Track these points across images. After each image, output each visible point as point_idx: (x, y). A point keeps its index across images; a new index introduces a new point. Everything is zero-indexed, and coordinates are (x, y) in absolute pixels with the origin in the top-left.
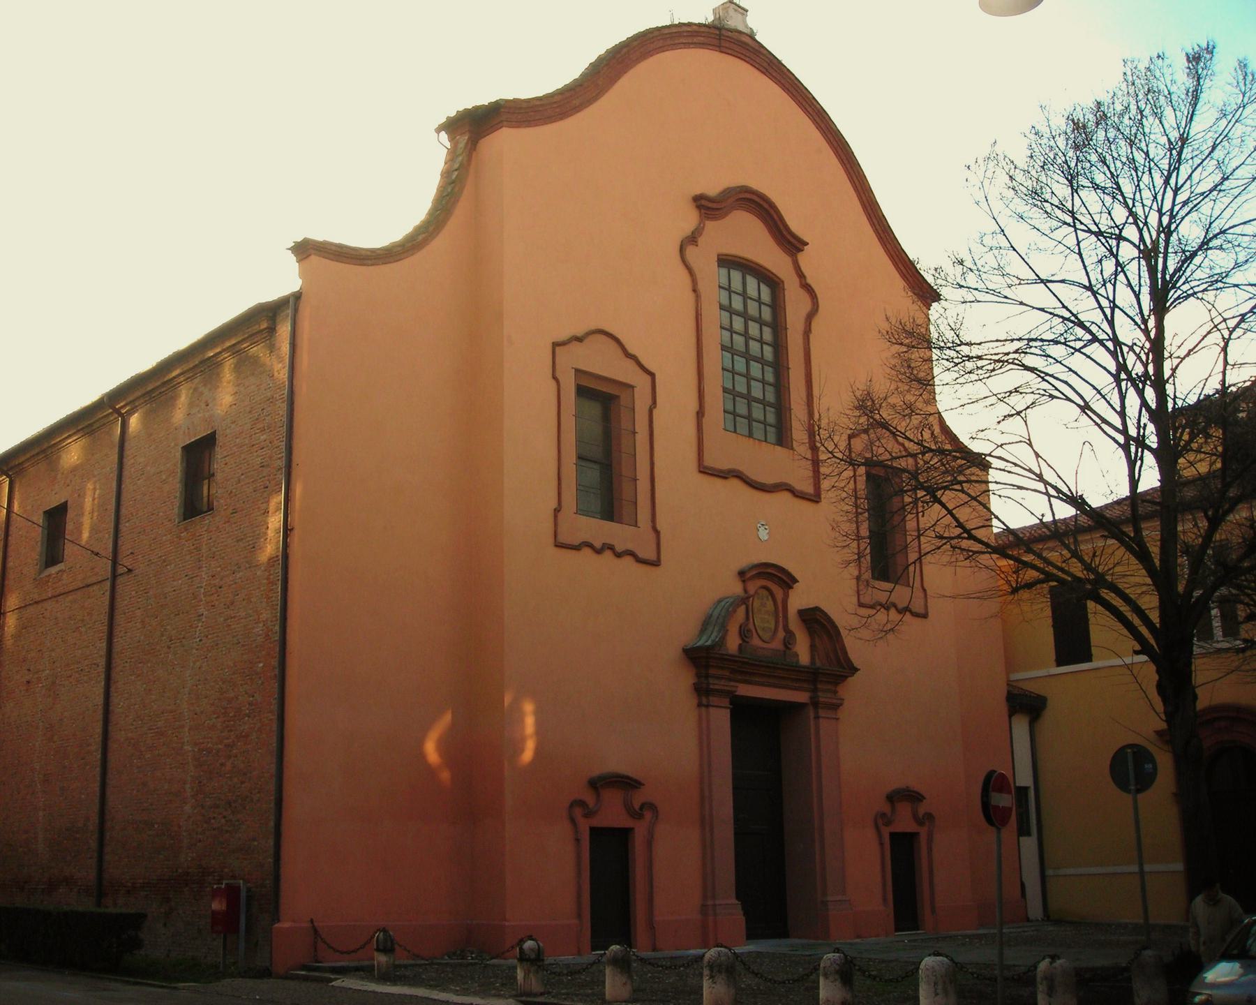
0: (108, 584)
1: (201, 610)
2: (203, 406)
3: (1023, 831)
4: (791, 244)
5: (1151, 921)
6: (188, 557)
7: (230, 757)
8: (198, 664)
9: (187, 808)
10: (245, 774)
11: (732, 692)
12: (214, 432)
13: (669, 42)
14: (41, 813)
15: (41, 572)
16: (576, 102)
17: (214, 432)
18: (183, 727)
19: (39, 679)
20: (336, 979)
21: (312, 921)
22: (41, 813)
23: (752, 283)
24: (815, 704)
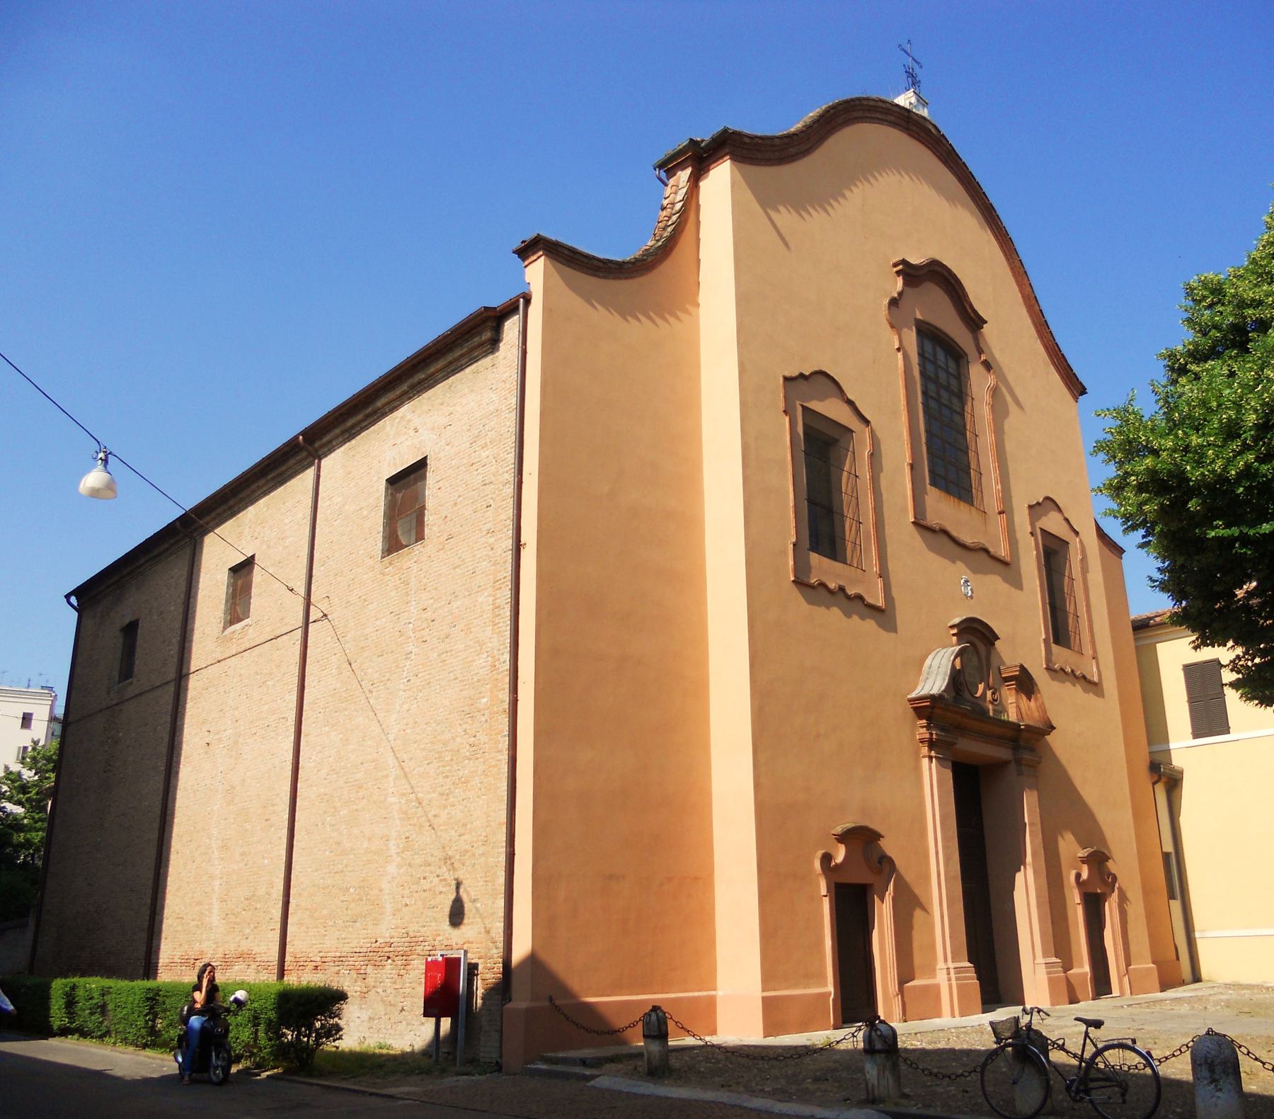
0: (299, 633)
1: (411, 648)
2: (412, 433)
3: (1172, 896)
4: (975, 322)
6: (393, 594)
7: (445, 807)
8: (406, 707)
9: (392, 869)
10: (464, 825)
11: (269, 1023)
12: (425, 458)
13: (868, 114)
14: (217, 882)
15: (225, 628)
16: (793, 150)
17: (425, 458)
18: (387, 776)
19: (220, 740)
20: (593, 1077)
21: (551, 999)
22: (217, 882)
23: (941, 355)
24: (1018, 762)
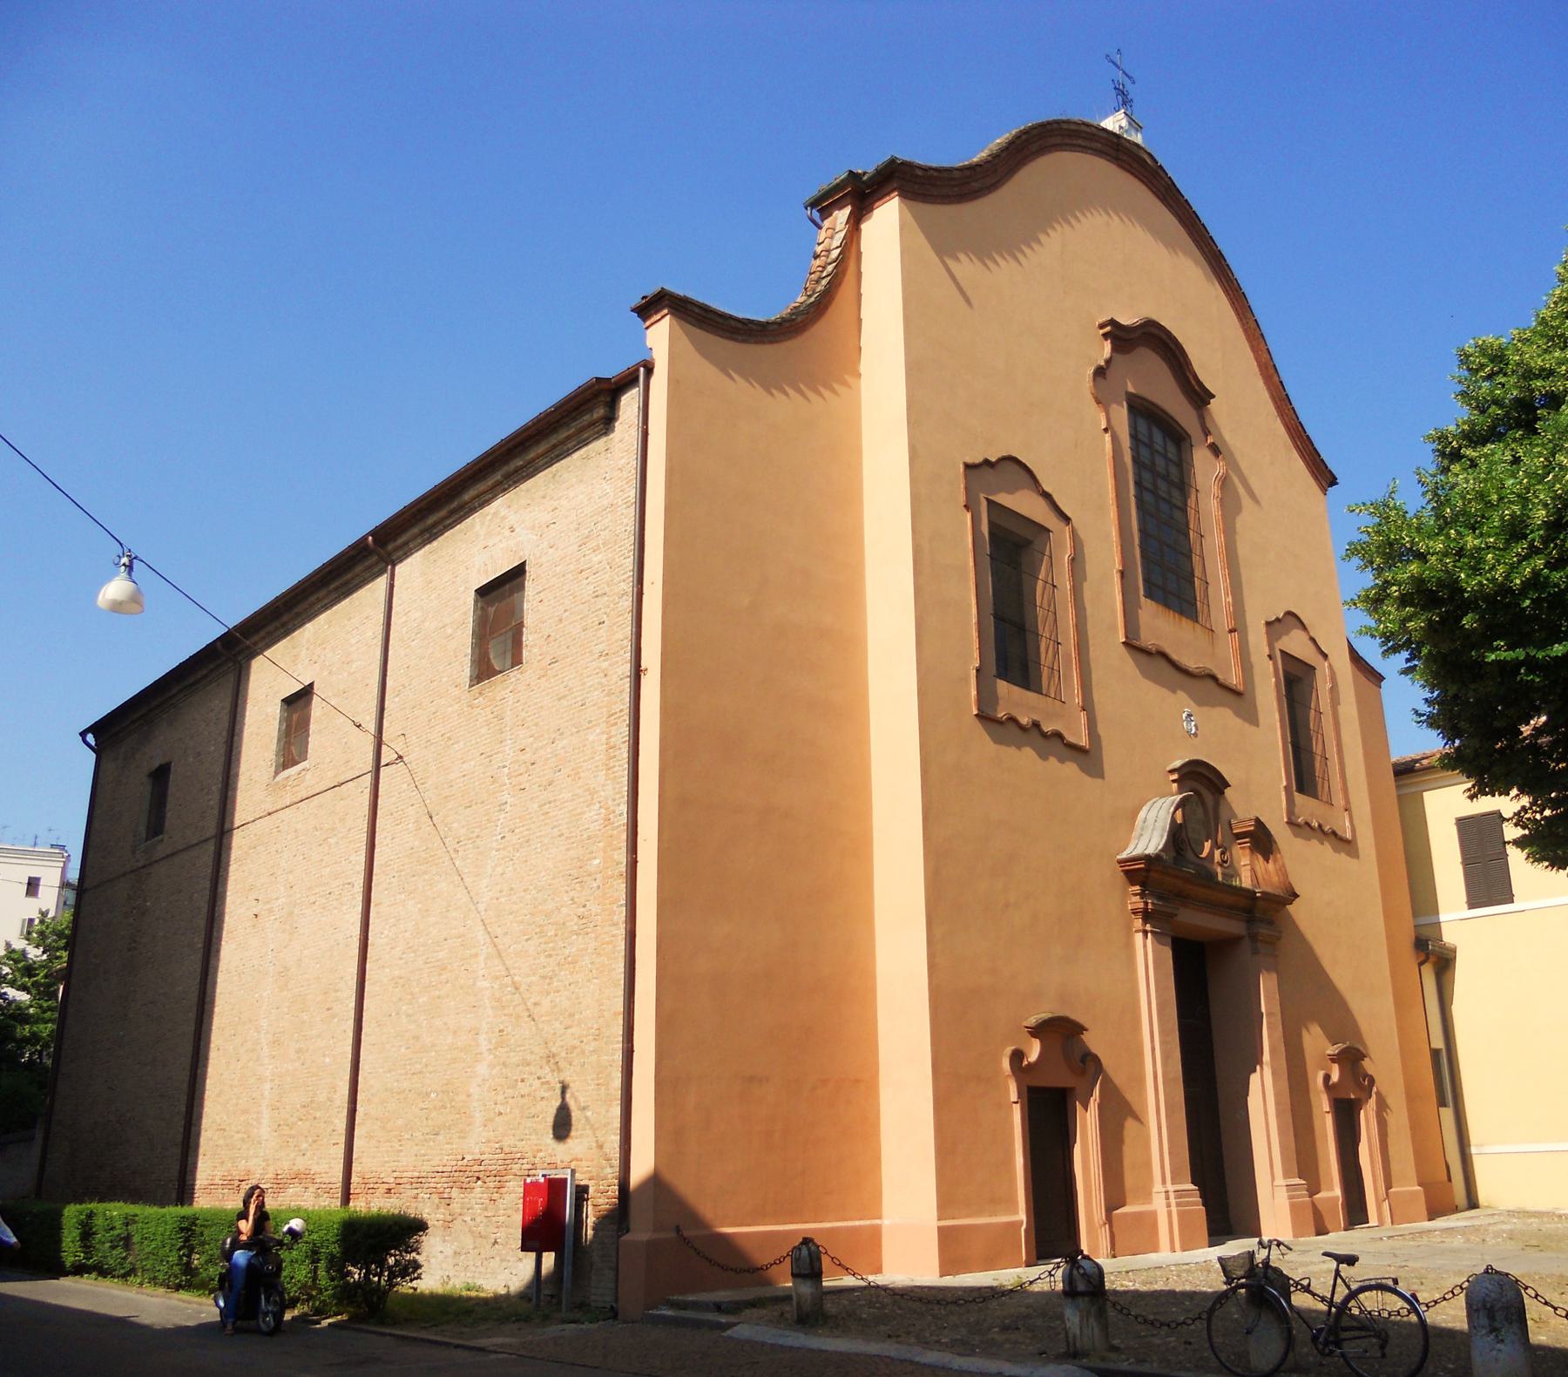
0: (368, 779)
1: (506, 797)
2: (507, 533)
3: (1442, 1103)
4: (1199, 396)
5: (533, 1255)
6: (484, 730)
8: (500, 870)
9: (482, 1069)
10: (572, 1015)
12: (524, 564)
13: (1068, 141)
14: (267, 1086)
15: (277, 773)
16: (976, 185)
17: (524, 564)
18: (476, 955)
19: (270, 911)
21: (678, 1230)
22: (267, 1086)
23: (1158, 437)
24: (1253, 937)
